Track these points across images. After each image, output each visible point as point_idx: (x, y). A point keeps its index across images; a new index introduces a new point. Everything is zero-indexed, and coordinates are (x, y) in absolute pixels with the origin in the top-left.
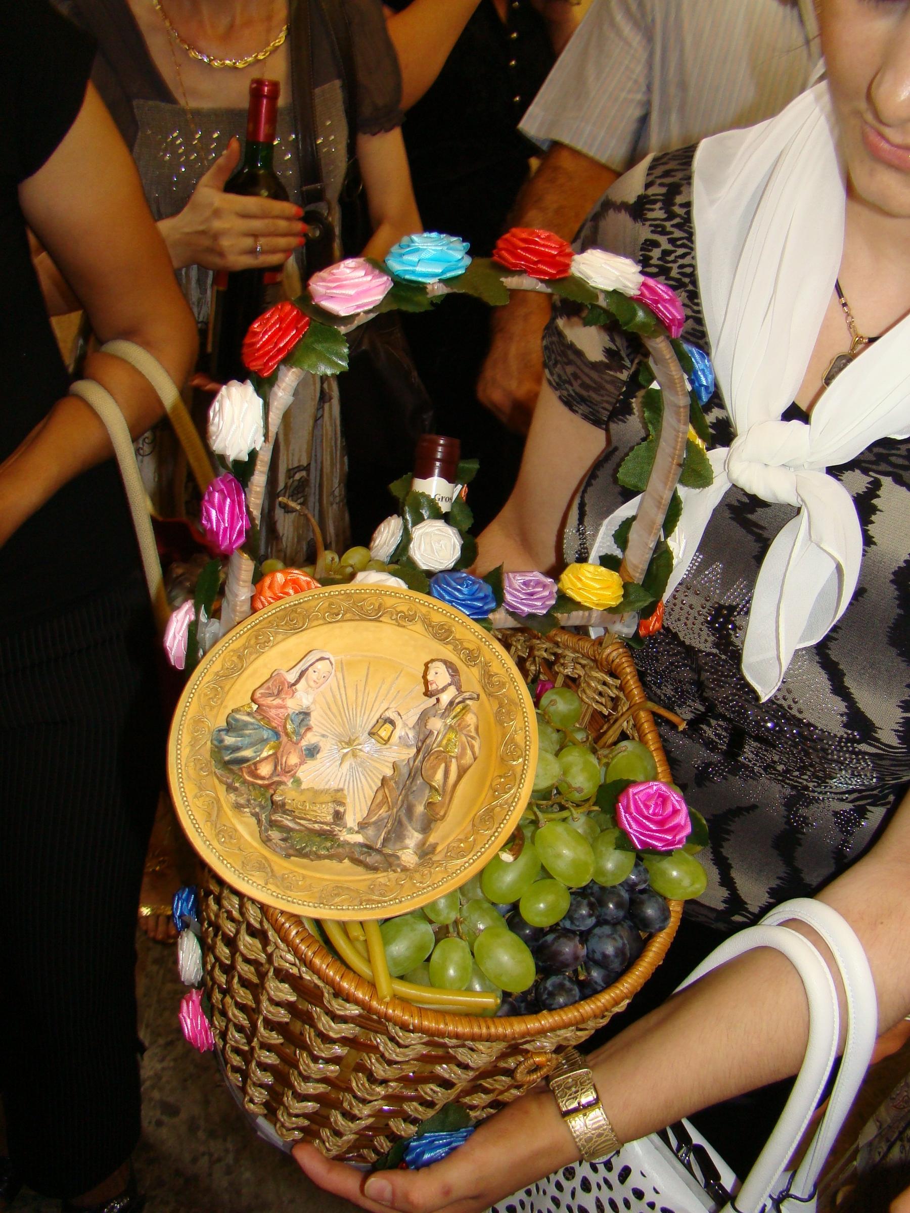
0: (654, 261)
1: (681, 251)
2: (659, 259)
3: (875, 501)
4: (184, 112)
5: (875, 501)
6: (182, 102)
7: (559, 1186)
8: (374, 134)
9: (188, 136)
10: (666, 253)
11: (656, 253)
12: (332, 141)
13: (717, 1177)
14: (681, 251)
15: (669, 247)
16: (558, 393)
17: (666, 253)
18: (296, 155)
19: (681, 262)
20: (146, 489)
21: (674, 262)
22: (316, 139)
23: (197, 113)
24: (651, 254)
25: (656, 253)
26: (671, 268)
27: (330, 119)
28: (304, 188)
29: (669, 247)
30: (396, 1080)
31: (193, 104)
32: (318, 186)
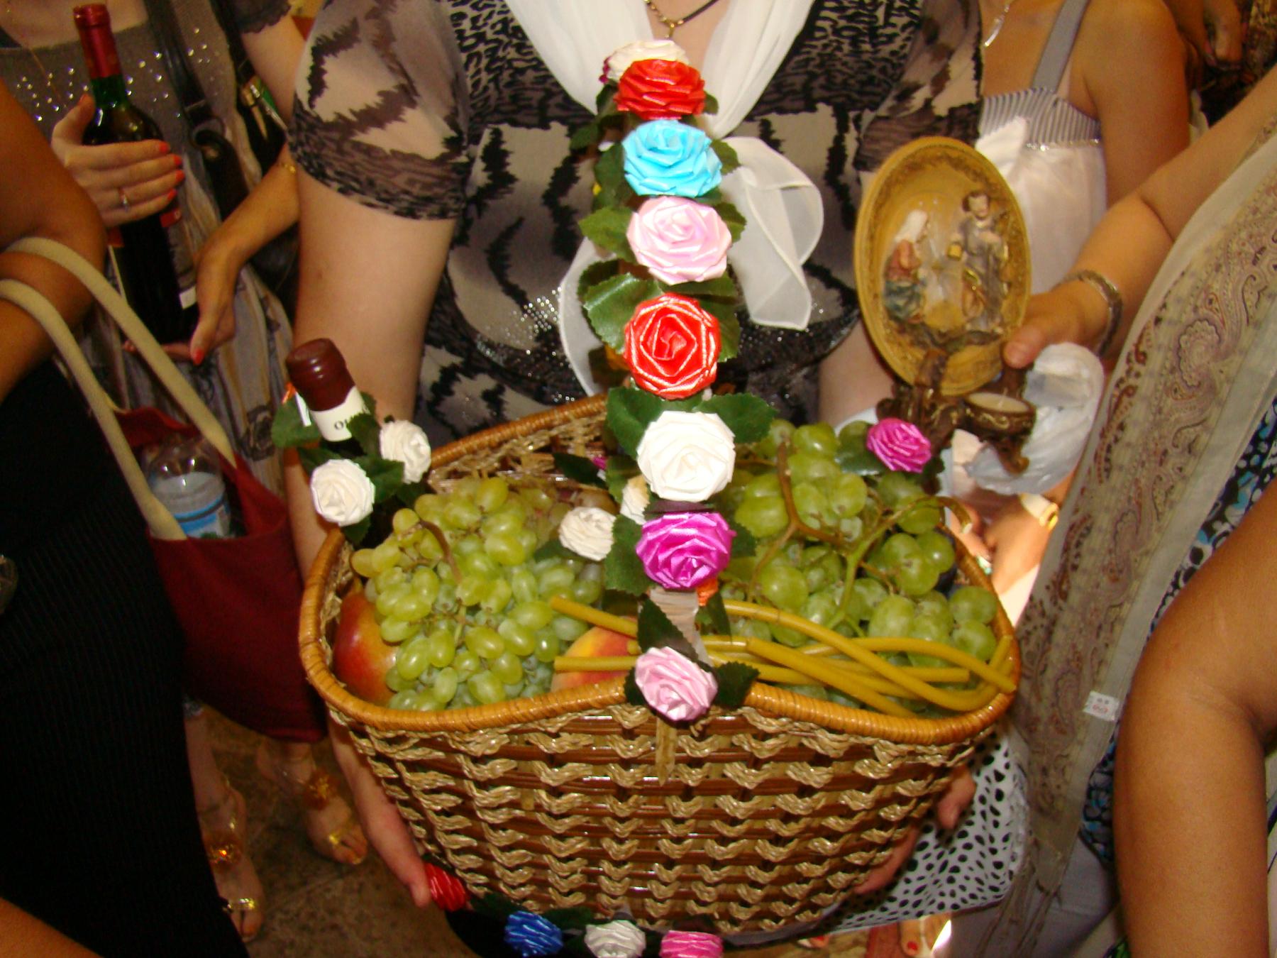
0: (468, 33)
1: (486, 12)
2: (472, 28)
3: (504, 147)
4: (27, 54)
5: (504, 147)
6: (22, 42)
7: (904, 903)
8: (259, 30)
9: (39, 81)
10: (475, 20)
11: (466, 25)
12: (208, 49)
13: (880, 828)
14: (486, 12)
15: (475, 13)
16: (393, 208)
17: (475, 20)
18: (166, 72)
19: (490, 22)
20: (905, 717)
21: (485, 24)
22: (186, 52)
23: (43, 52)
24: (462, 27)
25: (466, 25)
26: (484, 33)
27: (197, 26)
28: (187, 109)
29: (475, 13)
30: (692, 817)
31: (34, 44)
32: (202, 103)
